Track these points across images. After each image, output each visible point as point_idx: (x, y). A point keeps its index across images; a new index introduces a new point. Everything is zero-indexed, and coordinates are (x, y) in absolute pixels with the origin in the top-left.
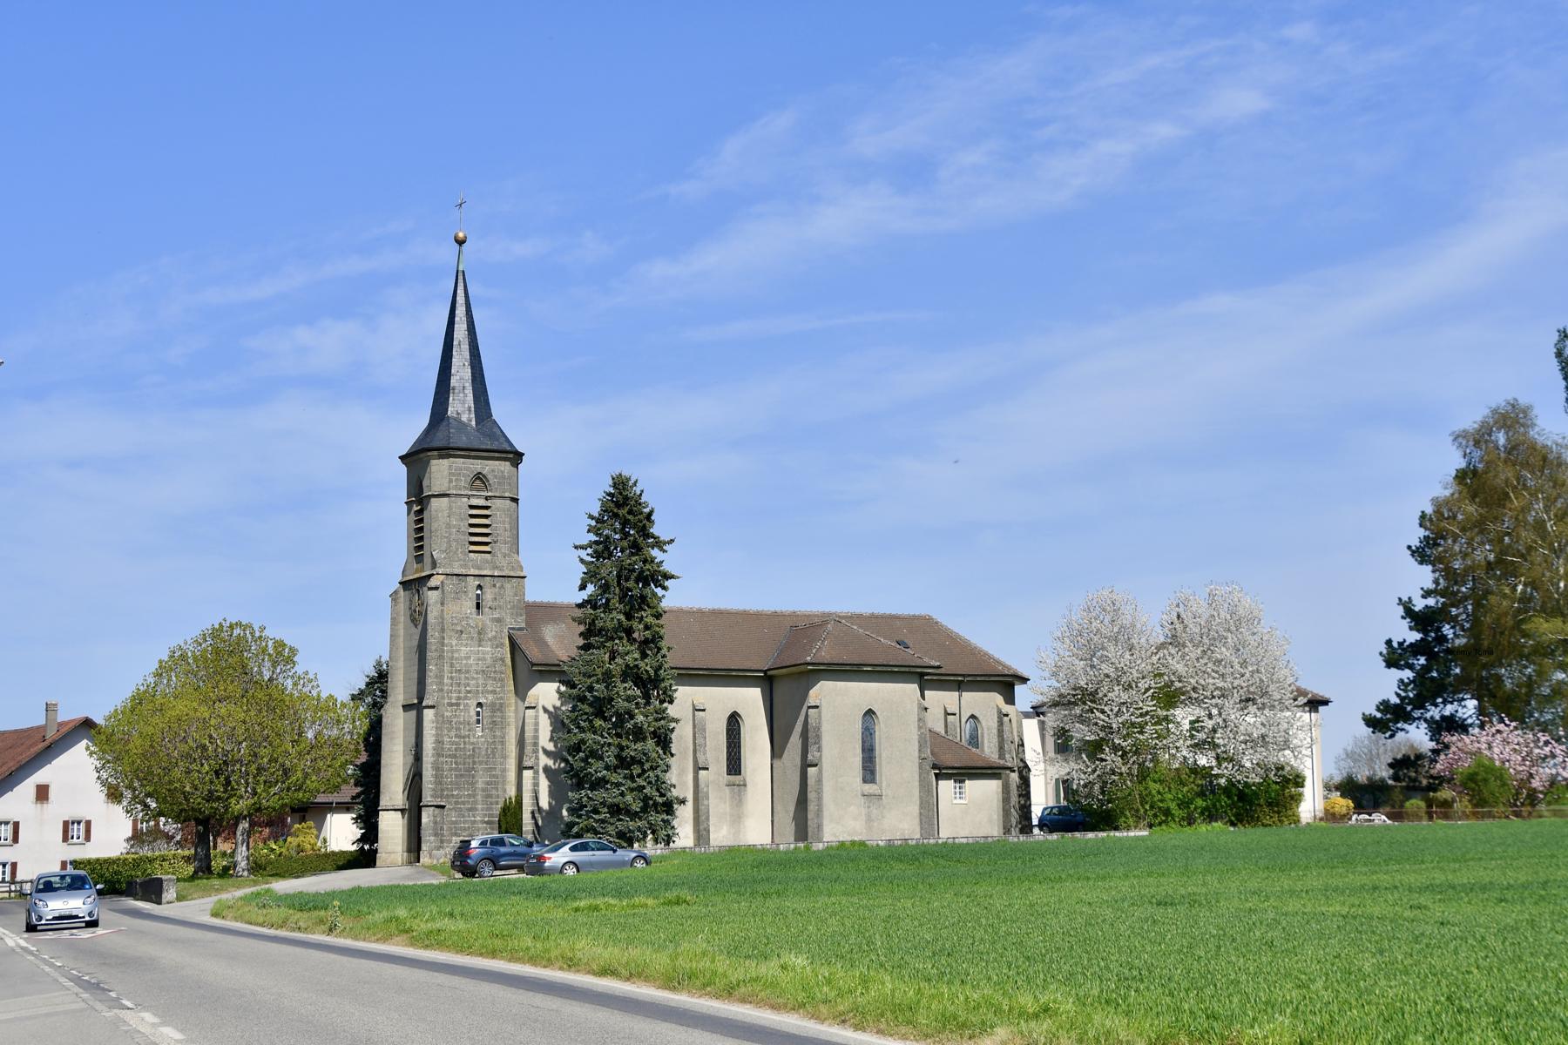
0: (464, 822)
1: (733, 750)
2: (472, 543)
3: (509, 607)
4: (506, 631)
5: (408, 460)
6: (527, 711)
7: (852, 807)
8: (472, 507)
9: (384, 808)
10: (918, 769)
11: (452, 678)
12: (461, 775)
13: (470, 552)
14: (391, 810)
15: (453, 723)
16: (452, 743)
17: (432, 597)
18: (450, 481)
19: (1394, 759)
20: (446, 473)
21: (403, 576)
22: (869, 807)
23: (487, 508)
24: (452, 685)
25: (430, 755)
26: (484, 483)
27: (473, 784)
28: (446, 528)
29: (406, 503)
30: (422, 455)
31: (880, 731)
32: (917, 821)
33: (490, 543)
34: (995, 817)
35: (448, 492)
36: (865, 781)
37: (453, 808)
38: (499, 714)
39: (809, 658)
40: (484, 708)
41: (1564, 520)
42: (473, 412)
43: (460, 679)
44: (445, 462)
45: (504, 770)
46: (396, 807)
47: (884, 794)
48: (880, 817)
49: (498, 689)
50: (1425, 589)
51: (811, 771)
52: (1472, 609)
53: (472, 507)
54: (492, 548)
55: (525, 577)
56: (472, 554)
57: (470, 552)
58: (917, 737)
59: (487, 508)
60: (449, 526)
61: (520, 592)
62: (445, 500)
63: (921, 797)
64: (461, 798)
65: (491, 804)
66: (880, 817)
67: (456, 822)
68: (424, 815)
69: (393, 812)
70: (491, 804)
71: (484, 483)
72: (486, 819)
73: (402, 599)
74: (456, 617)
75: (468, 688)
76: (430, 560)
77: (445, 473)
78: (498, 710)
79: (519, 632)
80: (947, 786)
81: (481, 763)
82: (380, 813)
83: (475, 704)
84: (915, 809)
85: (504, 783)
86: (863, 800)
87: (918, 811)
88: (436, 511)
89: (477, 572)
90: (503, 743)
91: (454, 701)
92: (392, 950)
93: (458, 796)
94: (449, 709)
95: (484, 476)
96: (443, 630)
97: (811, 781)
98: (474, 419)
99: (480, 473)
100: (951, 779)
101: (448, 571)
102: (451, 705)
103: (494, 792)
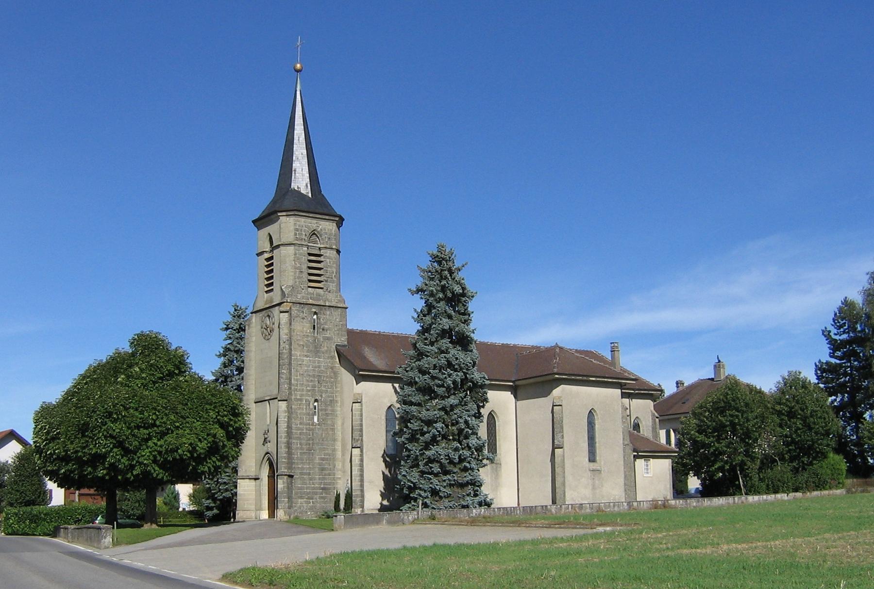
0: (307, 488)
1: (491, 438)
4: (334, 347)
6: (354, 404)
7: (583, 479)
8: (310, 254)
12: (304, 453)
13: (309, 287)
14: (247, 479)
20: (292, 228)
22: (594, 479)
24: (297, 386)
25: (284, 437)
32: (623, 489)
33: (322, 281)
34: (668, 486)
36: (590, 461)
37: (299, 478)
38: (329, 408)
39: (299, 296)
40: (320, 403)
42: (309, 187)
44: (292, 220)
45: (334, 450)
46: (250, 477)
47: (603, 469)
48: (600, 487)
51: (558, 451)
52: (133, 480)
53: (310, 254)
55: (346, 308)
56: (310, 289)
57: (309, 287)
58: (621, 430)
59: (320, 256)
61: (344, 317)
63: (625, 472)
66: (600, 487)
68: (280, 482)
69: (248, 480)
75: (308, 388)
76: (280, 293)
79: (343, 348)
80: (640, 463)
81: (318, 444)
83: (313, 400)
84: (621, 480)
85: (334, 459)
86: (589, 473)
87: (623, 482)
90: (333, 430)
91: (298, 397)
93: (303, 468)
94: (295, 403)
95: (318, 232)
96: (290, 344)
97: (558, 460)
100: (642, 458)
101: (294, 300)
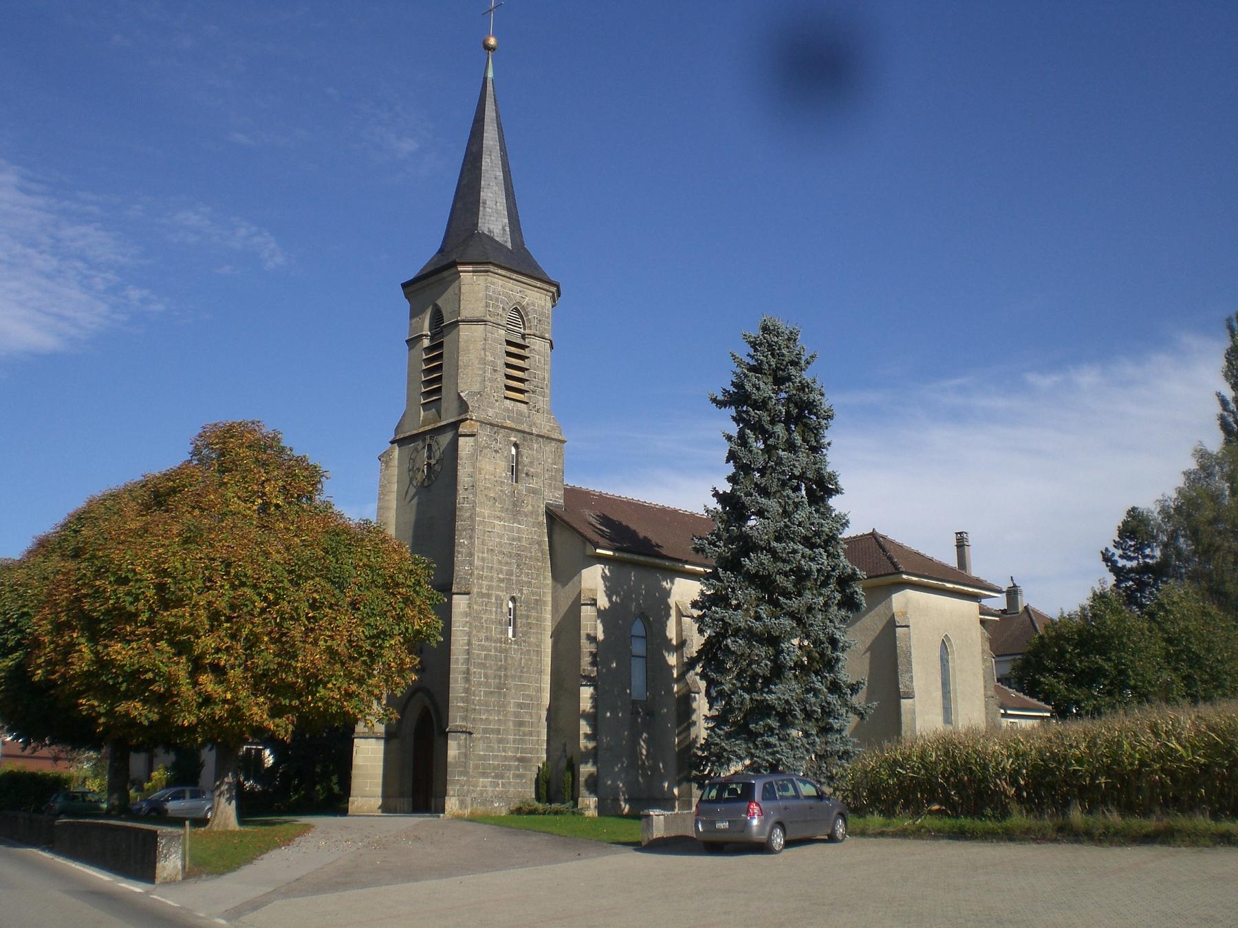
0: (495, 757)
9: (361, 735)
10: (984, 710)
11: (483, 559)
15: (483, 621)
18: (487, 306)
19: (695, 710)
23: (523, 347)
26: (522, 317)
27: (504, 706)
28: (479, 363)
29: (407, 341)
30: (445, 274)
31: (954, 662)
38: (534, 614)
41: (953, 562)
58: (982, 672)
60: (483, 361)
62: (481, 328)
64: (490, 724)
65: (524, 734)
67: (484, 758)
70: (524, 734)
71: (522, 317)
72: (519, 755)
73: (396, 462)
75: (501, 576)
78: (533, 608)
81: (513, 677)
89: (513, 425)
91: (484, 591)
92: (149, 826)
98: (509, 240)
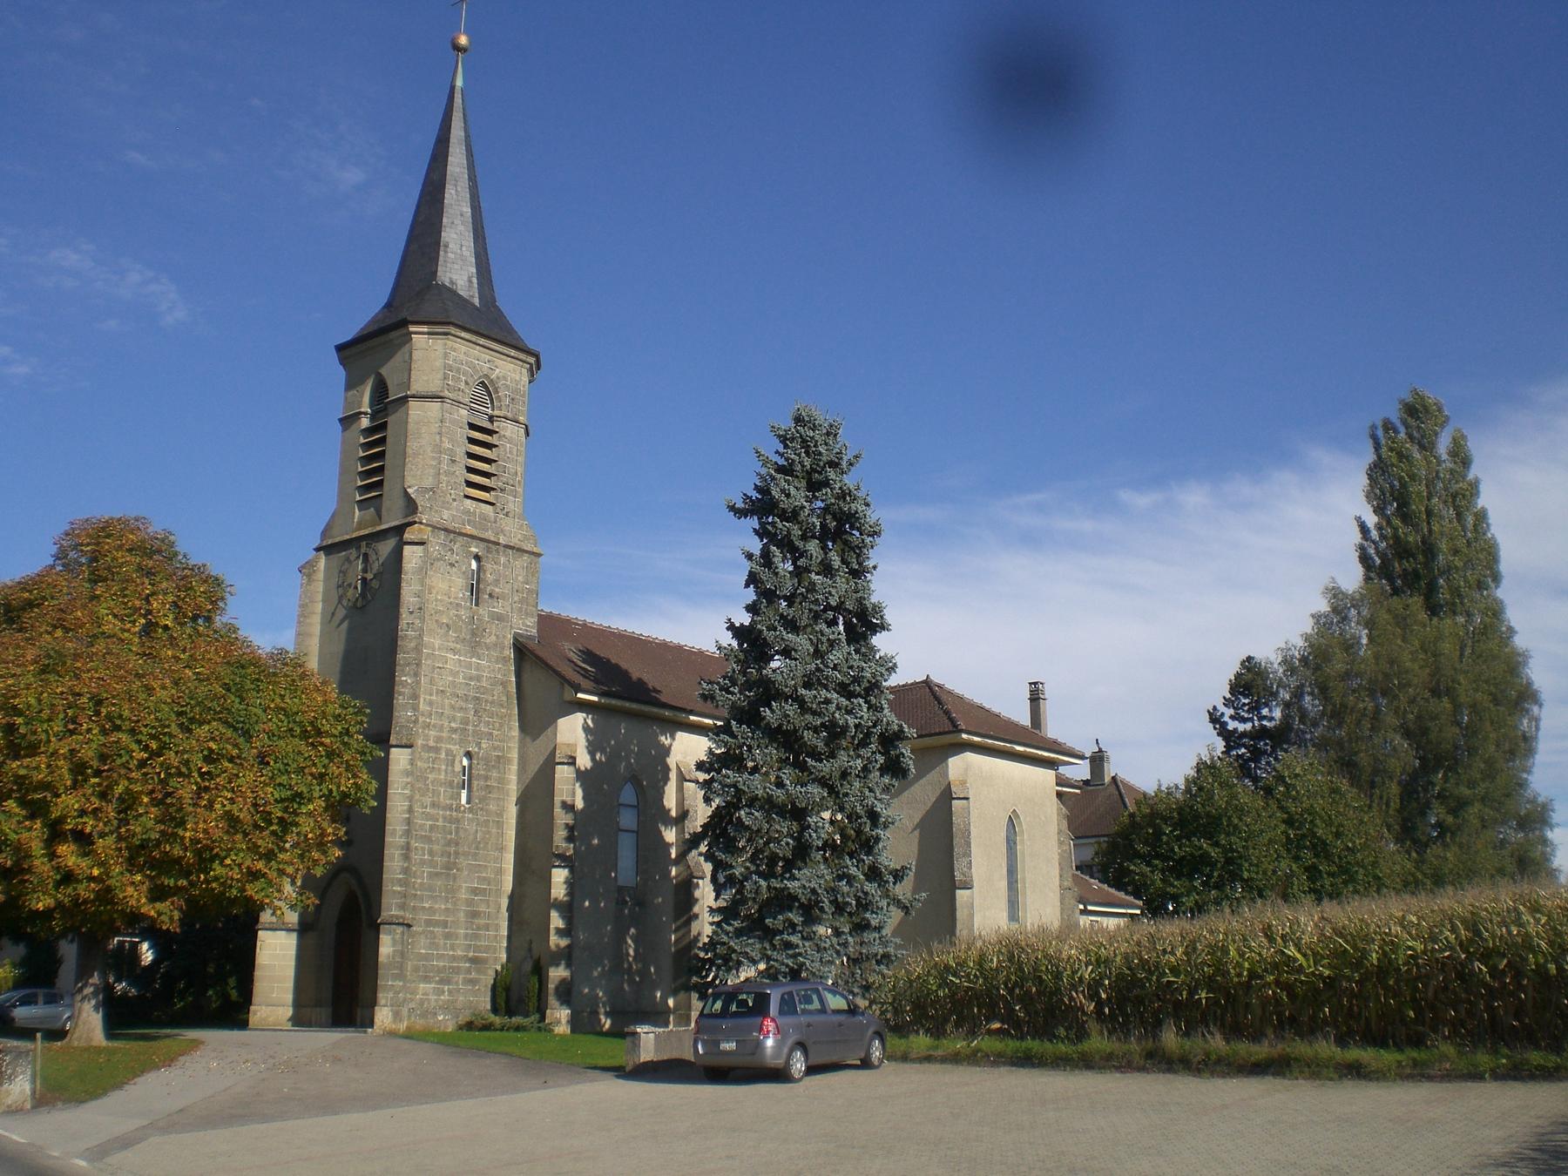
2: (470, 484)
3: (516, 599)
5: (347, 352)
12: (437, 874)
16: (428, 817)
17: (411, 555)
18: (445, 377)
20: (439, 363)
21: (322, 541)
26: (490, 395)
30: (393, 335)
35: (442, 394)
37: (423, 932)
43: (443, 707)
49: (495, 733)
50: (1111, 770)
54: (497, 497)
60: (439, 450)
65: (479, 928)
67: (427, 957)
72: (471, 954)
73: (321, 575)
74: (441, 601)
75: (453, 725)
77: (438, 364)
81: (466, 854)
82: (260, 932)
88: (417, 423)
91: (431, 743)
93: (432, 910)
98: (477, 295)
99: (486, 376)
102: (430, 749)
103: (482, 908)
